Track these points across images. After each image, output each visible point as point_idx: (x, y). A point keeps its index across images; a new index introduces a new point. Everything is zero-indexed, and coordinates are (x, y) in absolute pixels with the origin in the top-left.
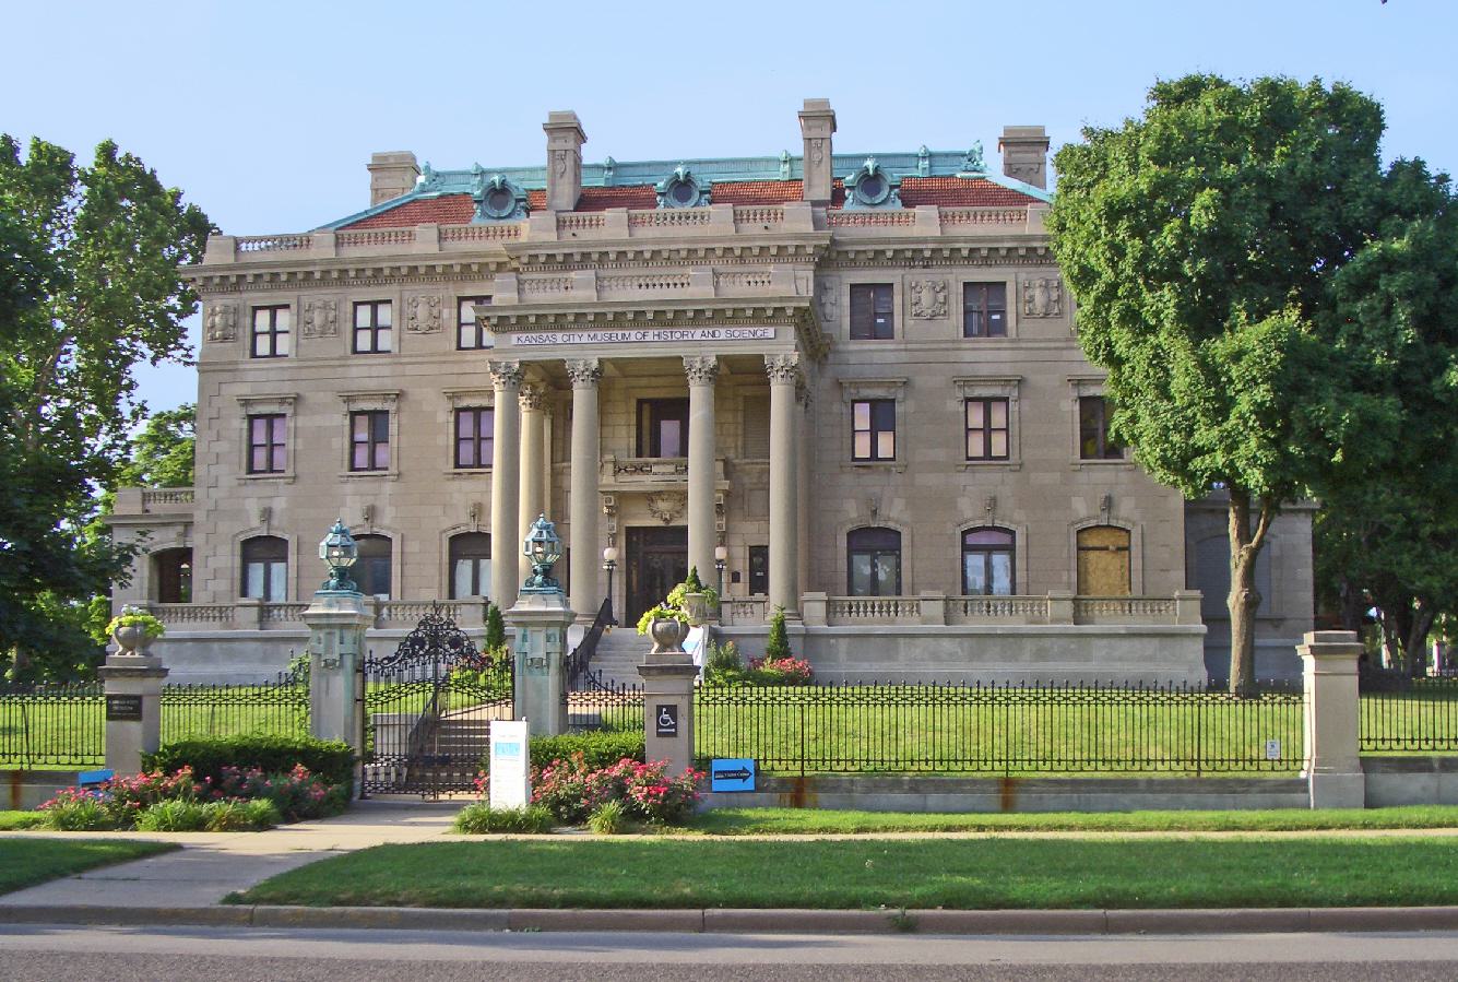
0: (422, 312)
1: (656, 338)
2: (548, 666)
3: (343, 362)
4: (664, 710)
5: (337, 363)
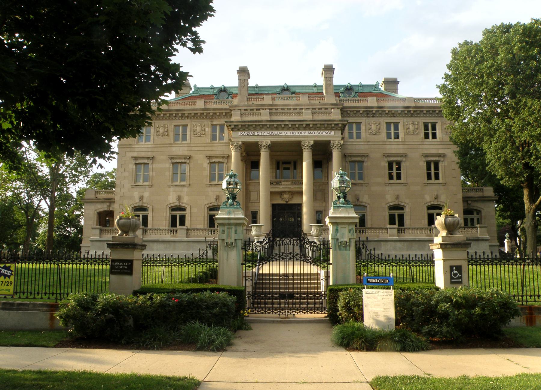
0: (198, 129)
1: (292, 134)
2: (350, 246)
3: (170, 146)
4: (454, 268)
5: (168, 146)
